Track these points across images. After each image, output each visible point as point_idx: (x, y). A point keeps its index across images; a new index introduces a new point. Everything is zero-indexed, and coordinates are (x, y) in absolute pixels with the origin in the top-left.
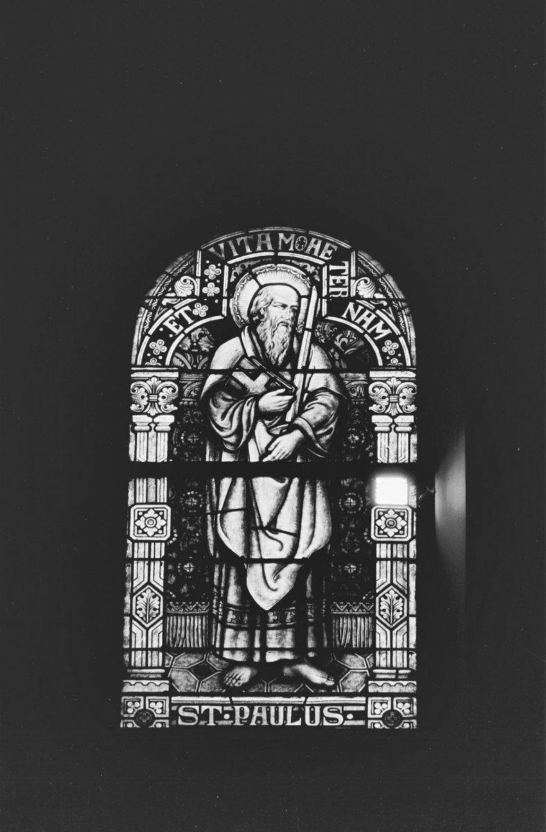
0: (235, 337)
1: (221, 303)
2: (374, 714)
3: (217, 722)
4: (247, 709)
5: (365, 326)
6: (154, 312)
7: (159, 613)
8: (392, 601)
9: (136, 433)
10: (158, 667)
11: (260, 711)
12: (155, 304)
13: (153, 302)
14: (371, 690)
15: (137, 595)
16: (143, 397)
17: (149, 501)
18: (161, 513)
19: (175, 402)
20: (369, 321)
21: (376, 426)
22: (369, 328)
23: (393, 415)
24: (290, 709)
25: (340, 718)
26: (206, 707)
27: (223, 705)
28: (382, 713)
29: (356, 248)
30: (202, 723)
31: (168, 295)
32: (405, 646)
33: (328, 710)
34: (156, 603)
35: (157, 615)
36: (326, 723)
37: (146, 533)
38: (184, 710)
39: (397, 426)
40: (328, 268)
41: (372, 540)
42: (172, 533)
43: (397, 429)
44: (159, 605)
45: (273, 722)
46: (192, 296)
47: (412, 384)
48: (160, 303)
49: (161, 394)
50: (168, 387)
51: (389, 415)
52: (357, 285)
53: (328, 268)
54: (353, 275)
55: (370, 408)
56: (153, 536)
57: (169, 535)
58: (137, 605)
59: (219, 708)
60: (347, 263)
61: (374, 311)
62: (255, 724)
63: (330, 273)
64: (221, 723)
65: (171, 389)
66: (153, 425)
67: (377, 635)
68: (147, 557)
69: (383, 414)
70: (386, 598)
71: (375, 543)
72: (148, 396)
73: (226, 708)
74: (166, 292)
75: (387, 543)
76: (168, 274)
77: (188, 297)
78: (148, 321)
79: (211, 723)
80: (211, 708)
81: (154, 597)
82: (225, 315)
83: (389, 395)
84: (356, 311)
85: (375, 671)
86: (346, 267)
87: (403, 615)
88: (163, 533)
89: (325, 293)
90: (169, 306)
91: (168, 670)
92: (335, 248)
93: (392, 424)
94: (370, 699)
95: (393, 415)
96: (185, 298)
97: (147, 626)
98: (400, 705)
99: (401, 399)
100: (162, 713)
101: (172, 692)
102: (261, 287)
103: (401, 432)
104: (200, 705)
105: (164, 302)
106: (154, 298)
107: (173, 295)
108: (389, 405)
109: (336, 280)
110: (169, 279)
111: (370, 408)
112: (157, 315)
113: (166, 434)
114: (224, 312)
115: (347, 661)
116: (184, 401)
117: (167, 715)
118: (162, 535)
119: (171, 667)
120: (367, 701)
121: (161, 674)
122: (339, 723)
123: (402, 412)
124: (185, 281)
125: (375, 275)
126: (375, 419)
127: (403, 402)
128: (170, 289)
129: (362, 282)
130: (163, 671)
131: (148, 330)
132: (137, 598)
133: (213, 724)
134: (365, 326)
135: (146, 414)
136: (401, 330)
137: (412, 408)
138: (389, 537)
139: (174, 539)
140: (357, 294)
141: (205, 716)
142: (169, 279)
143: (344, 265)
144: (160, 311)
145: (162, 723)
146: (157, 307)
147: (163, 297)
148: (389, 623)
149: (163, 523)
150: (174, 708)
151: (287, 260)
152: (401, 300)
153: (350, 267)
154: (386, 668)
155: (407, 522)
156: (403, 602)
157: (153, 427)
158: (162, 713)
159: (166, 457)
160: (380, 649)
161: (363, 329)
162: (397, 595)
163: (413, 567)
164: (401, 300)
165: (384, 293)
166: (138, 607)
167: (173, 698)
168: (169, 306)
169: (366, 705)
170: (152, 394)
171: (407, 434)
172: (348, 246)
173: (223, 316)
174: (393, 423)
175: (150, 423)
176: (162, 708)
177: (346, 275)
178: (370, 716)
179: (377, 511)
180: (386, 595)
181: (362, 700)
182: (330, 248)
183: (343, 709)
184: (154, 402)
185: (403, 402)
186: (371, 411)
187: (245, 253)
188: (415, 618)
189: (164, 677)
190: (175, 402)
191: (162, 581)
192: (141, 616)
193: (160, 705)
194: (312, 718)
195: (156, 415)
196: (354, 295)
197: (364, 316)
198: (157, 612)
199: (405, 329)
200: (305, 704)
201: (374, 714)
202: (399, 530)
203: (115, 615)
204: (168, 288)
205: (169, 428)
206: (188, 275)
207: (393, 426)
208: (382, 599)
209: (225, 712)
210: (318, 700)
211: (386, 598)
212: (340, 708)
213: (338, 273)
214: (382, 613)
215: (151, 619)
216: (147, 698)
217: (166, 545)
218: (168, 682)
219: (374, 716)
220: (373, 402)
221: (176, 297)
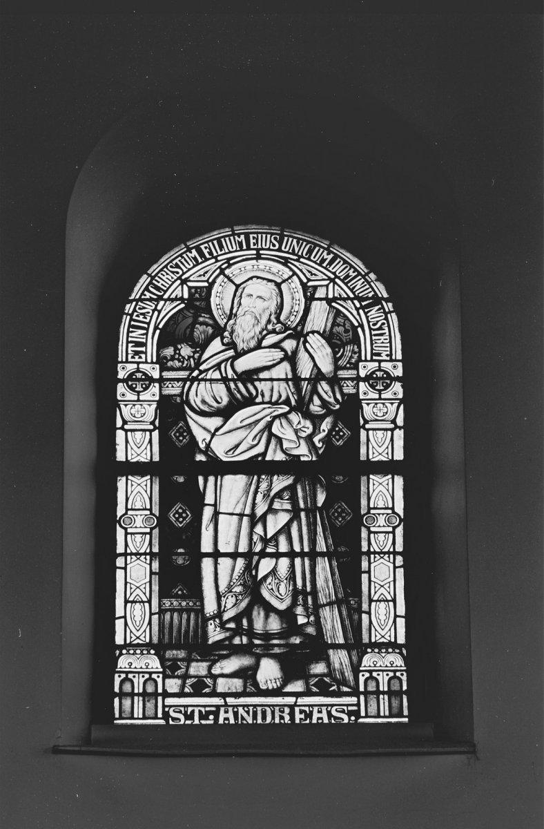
0: (404, 423)
11: (320, 712)
17: (124, 557)
23: (398, 429)
25: (182, 717)
30: (188, 722)
33: (174, 711)
45: (260, 721)
59: (203, 709)
64: (203, 722)
76: (148, 274)
79: (197, 721)
95: (398, 429)
102: (238, 286)
104: (185, 706)
109: (254, 243)
115: (253, 659)
141: (191, 717)
150: (167, 709)
163: (120, 549)
188: (403, 620)
194: (264, 717)
200: (296, 704)
210: (270, 701)
212: (345, 708)
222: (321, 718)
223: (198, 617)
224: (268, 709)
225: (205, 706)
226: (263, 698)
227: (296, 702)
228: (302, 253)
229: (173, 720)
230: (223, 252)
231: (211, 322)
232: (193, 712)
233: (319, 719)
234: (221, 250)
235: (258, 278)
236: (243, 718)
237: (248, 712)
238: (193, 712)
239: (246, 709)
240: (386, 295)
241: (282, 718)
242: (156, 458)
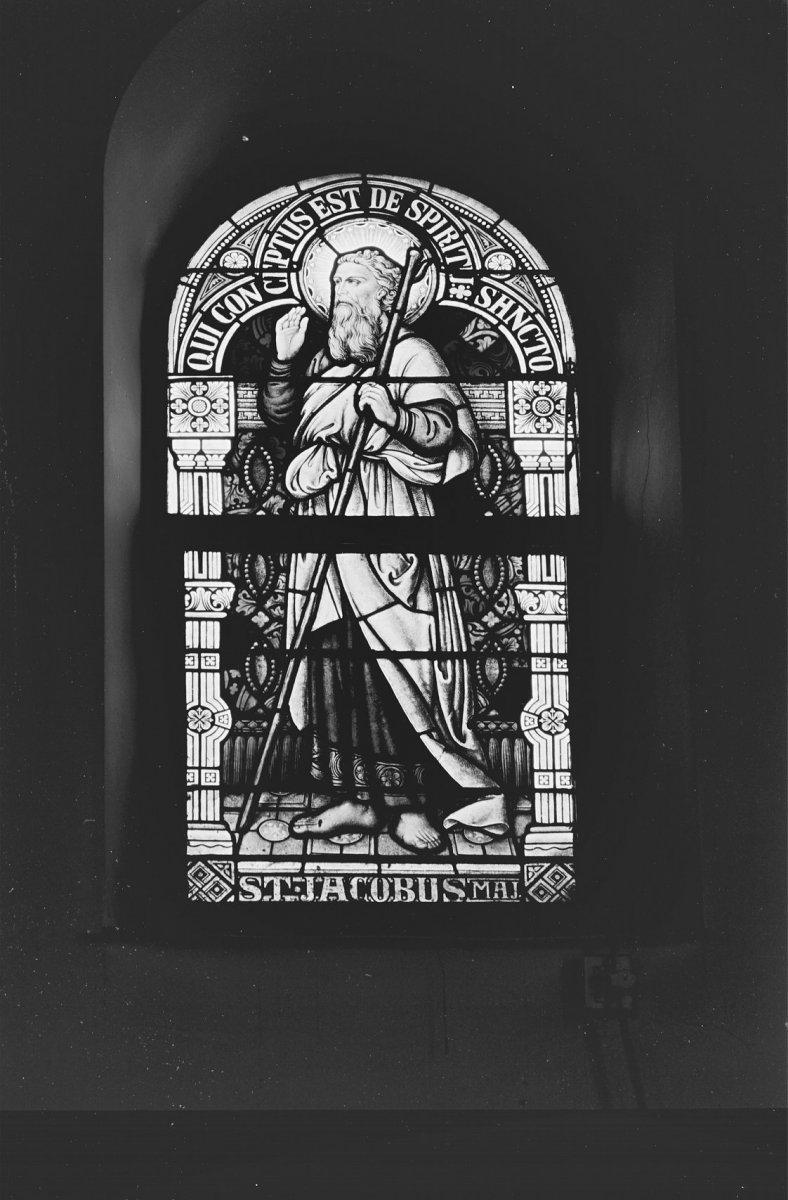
5: (500, 315)
20: (506, 308)
22: (505, 317)
24: (354, 882)
26: (272, 878)
27: (292, 875)
30: (266, 898)
45: (311, 897)
62: (325, 900)
73: (295, 879)
84: (252, 291)
92: (402, 195)
104: (262, 875)
129: (535, 607)
134: (500, 315)
152: (544, 273)
161: (497, 318)
164: (544, 273)
177: (279, 233)
182: (396, 197)
183: (292, 880)
194: (380, 894)
197: (500, 302)
209: (294, 884)
222: (336, 895)
223: (524, 761)
224: (384, 881)
226: (339, 864)
227: (303, 868)
228: (441, 219)
232: (271, 883)
233: (330, 895)
238: (271, 883)
240: (543, 267)
241: (404, 894)
242: (575, 510)
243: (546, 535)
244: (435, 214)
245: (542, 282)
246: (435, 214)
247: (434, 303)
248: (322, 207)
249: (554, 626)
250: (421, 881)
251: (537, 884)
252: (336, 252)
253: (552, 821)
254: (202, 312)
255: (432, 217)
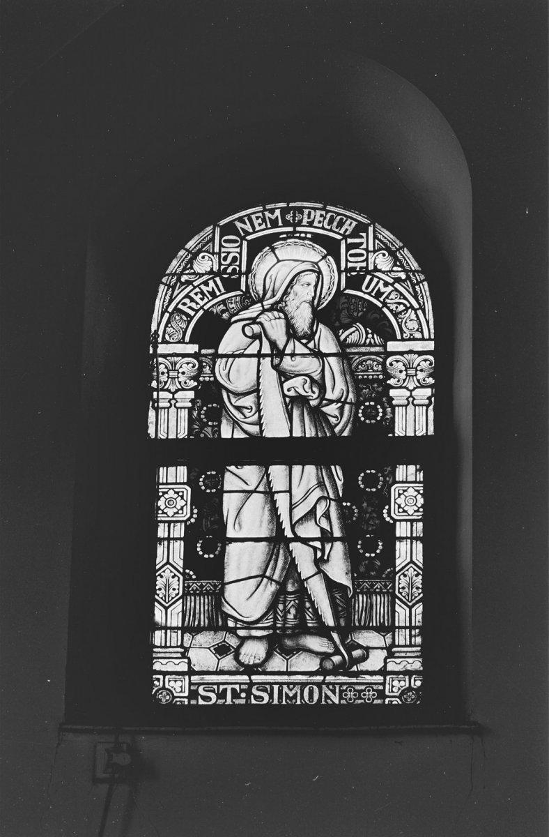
1: (239, 279)
2: (392, 692)
3: (234, 700)
4: (316, 689)
6: (174, 288)
7: (178, 594)
8: (168, 580)
9: (157, 409)
10: (177, 647)
12: (174, 281)
13: (172, 278)
14: (390, 667)
15: (400, 573)
16: (401, 371)
17: (168, 482)
18: (181, 494)
19: (195, 378)
21: (394, 399)
26: (225, 686)
28: (400, 691)
29: (373, 223)
30: (221, 702)
31: (187, 272)
32: (408, 625)
34: (175, 583)
35: (177, 595)
36: (253, 701)
37: (166, 513)
38: (258, 689)
39: (414, 399)
40: (346, 242)
41: (392, 518)
42: (192, 513)
43: (415, 402)
44: (179, 585)
46: (211, 272)
47: (431, 358)
48: (179, 280)
49: (419, 368)
50: (188, 363)
51: (407, 389)
52: (375, 258)
53: (346, 242)
54: (371, 248)
55: (388, 382)
56: (173, 516)
57: (189, 515)
58: (399, 584)
60: (364, 235)
61: (392, 285)
63: (349, 247)
64: (237, 701)
65: (428, 362)
66: (173, 402)
67: (397, 614)
68: (409, 535)
69: (401, 387)
70: (405, 576)
71: (395, 521)
72: (406, 370)
73: (244, 687)
74: (185, 269)
75: (406, 521)
77: (207, 273)
78: (168, 298)
79: (229, 701)
80: (229, 688)
81: (173, 577)
82: (244, 290)
83: (168, 371)
85: (394, 650)
86: (364, 240)
87: (178, 594)
88: (183, 513)
89: (343, 267)
90: (189, 283)
91: (187, 650)
93: (409, 397)
94: (388, 678)
96: (203, 275)
97: (167, 605)
98: (172, 683)
99: (418, 373)
100: (181, 692)
101: (191, 672)
103: (419, 405)
104: (218, 684)
105: (183, 279)
106: (173, 275)
107: (192, 271)
108: (406, 379)
109: (201, 299)
110: (188, 255)
111: (388, 382)
112: (176, 292)
113: (187, 410)
114: (243, 288)
116: (204, 377)
117: (186, 694)
118: (182, 515)
119: (190, 647)
120: (385, 679)
121: (181, 653)
122: (265, 701)
123: (180, 387)
124: (203, 257)
125: (394, 249)
126: (392, 393)
127: (182, 378)
128: (189, 266)
130: (182, 650)
131: (168, 307)
132: (399, 577)
133: (231, 703)
135: (405, 388)
136: (419, 304)
137: (431, 381)
138: (409, 515)
139: (195, 516)
140: (375, 267)
141: (222, 695)
142: (188, 255)
143: (362, 237)
144: (179, 288)
145: (181, 702)
146: (176, 284)
147: (182, 273)
148: (165, 601)
149: (183, 503)
150: (193, 688)
151: (281, 236)
153: (367, 239)
154: (161, 647)
155: (187, 502)
156: (179, 580)
157: (411, 400)
158: (181, 692)
159: (186, 433)
160: (400, 628)
162: (416, 573)
165: (402, 266)
166: (401, 586)
167: (192, 678)
168: (189, 283)
169: (384, 684)
170: (410, 368)
171: (404, 408)
172: (366, 221)
173: (242, 291)
174: (411, 396)
175: (170, 400)
176: (181, 687)
178: (387, 693)
179: (397, 490)
180: (162, 574)
181: (379, 678)
183: (240, 687)
184: (174, 378)
185: (182, 378)
186: (389, 384)
187: (277, 226)
189: (184, 656)
190: (195, 378)
191: (182, 562)
192: (161, 596)
193: (179, 683)
195: (177, 391)
196: (372, 268)
198: (177, 591)
199: (424, 302)
200: (323, 682)
201: (392, 692)
202: (419, 508)
203: (148, 596)
204: (186, 265)
205: (190, 405)
206: (207, 251)
207: (411, 399)
208: (402, 577)
209: (242, 691)
211: (405, 576)
212: (215, 687)
213: (357, 246)
214: (401, 590)
215: (413, 597)
216: (167, 677)
217: (185, 525)
218: (186, 660)
219: (392, 694)
220: (389, 376)
221: (194, 273)
225: (240, 684)
227: (324, 679)
229: (255, 699)
230: (337, 230)
231: (204, 249)
234: (337, 228)
235: (299, 274)
236: (327, 697)
237: (334, 692)
238: (225, 690)
239: (331, 687)
242: (431, 431)
243: (411, 449)
244: (310, 213)
245: (416, 279)
246: (310, 213)
247: (339, 292)
248: (260, 221)
249: (165, 481)
250: (276, 687)
251: (182, 699)
252: (277, 258)
253: (163, 645)
254: (204, 310)
255: (309, 218)
